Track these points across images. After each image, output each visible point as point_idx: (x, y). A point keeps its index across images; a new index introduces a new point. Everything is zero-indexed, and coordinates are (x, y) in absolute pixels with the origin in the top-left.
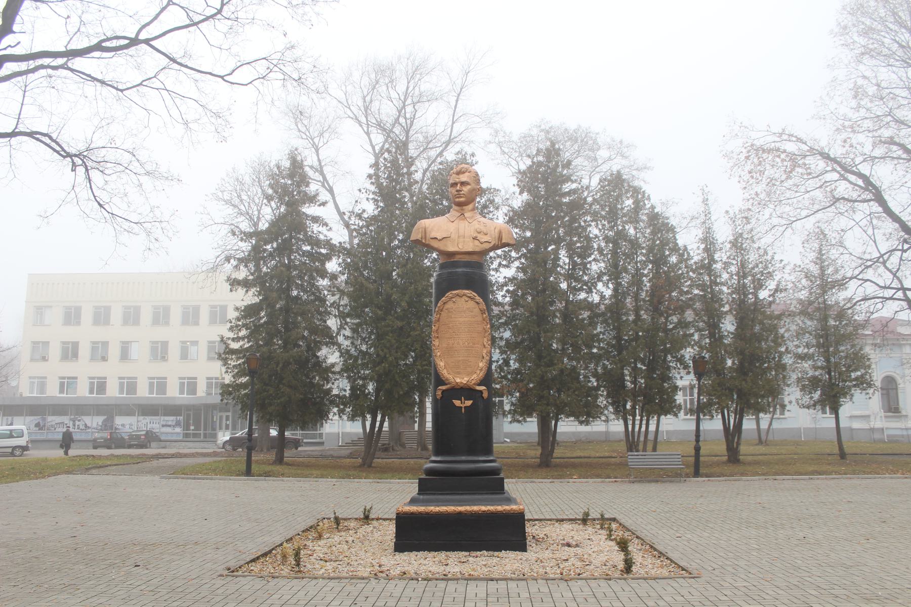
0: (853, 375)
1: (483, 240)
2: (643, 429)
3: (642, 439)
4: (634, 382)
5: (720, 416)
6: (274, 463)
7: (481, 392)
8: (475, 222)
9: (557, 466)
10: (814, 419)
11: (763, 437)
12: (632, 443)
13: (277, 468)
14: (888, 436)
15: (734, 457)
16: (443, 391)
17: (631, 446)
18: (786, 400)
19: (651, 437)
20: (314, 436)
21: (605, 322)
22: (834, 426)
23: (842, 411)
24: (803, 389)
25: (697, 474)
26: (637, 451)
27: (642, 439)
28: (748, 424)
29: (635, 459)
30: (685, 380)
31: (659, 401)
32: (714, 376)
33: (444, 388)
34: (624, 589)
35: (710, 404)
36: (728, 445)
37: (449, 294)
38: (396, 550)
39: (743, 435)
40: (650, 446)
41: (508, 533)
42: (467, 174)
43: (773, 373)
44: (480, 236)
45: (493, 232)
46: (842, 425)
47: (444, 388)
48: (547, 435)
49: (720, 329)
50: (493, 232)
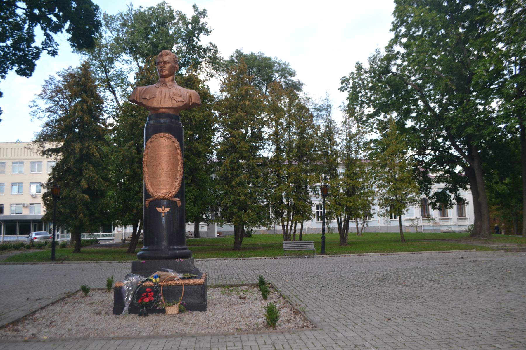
0: (409, 196)
1: (178, 100)
2: (293, 228)
3: (292, 233)
4: (288, 201)
5: (336, 220)
6: (74, 252)
7: (176, 202)
8: (173, 88)
9: (245, 249)
10: (387, 222)
11: (360, 232)
12: (287, 236)
13: (77, 255)
14: (424, 230)
15: (344, 243)
16: (150, 202)
17: (286, 237)
18: (372, 212)
19: (298, 232)
20: (110, 236)
21: (184, 40)
22: (399, 225)
23: (402, 216)
24: (380, 206)
25: (323, 252)
26: (290, 240)
27: (292, 233)
28: (352, 225)
29: (288, 246)
30: (316, 201)
31: (301, 212)
32: (332, 198)
33: (150, 199)
34: (275, 337)
35: (330, 214)
36: (340, 236)
37: (154, 136)
38: (114, 314)
39: (349, 231)
40: (297, 238)
41: (195, 300)
42: (168, 56)
43: (423, 135)
44: (176, 97)
45: (185, 95)
46: (403, 224)
47: (150, 199)
48: (239, 233)
49: (336, 170)
50: (185, 95)
